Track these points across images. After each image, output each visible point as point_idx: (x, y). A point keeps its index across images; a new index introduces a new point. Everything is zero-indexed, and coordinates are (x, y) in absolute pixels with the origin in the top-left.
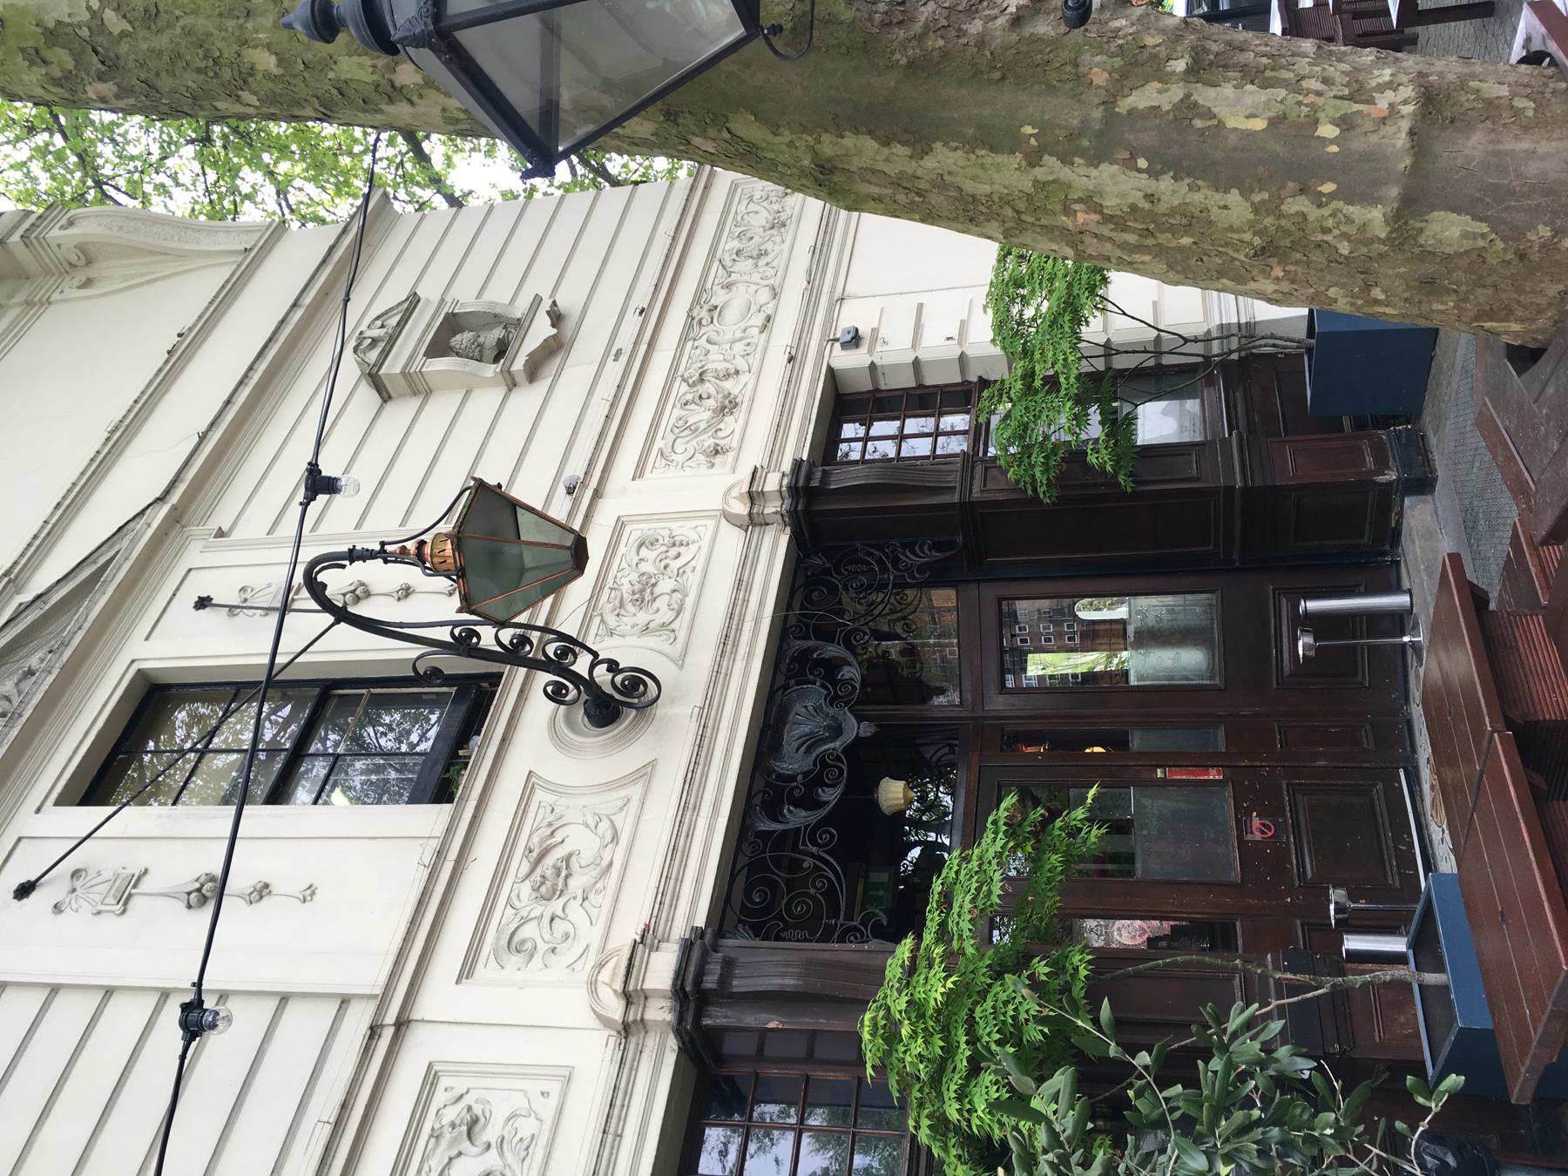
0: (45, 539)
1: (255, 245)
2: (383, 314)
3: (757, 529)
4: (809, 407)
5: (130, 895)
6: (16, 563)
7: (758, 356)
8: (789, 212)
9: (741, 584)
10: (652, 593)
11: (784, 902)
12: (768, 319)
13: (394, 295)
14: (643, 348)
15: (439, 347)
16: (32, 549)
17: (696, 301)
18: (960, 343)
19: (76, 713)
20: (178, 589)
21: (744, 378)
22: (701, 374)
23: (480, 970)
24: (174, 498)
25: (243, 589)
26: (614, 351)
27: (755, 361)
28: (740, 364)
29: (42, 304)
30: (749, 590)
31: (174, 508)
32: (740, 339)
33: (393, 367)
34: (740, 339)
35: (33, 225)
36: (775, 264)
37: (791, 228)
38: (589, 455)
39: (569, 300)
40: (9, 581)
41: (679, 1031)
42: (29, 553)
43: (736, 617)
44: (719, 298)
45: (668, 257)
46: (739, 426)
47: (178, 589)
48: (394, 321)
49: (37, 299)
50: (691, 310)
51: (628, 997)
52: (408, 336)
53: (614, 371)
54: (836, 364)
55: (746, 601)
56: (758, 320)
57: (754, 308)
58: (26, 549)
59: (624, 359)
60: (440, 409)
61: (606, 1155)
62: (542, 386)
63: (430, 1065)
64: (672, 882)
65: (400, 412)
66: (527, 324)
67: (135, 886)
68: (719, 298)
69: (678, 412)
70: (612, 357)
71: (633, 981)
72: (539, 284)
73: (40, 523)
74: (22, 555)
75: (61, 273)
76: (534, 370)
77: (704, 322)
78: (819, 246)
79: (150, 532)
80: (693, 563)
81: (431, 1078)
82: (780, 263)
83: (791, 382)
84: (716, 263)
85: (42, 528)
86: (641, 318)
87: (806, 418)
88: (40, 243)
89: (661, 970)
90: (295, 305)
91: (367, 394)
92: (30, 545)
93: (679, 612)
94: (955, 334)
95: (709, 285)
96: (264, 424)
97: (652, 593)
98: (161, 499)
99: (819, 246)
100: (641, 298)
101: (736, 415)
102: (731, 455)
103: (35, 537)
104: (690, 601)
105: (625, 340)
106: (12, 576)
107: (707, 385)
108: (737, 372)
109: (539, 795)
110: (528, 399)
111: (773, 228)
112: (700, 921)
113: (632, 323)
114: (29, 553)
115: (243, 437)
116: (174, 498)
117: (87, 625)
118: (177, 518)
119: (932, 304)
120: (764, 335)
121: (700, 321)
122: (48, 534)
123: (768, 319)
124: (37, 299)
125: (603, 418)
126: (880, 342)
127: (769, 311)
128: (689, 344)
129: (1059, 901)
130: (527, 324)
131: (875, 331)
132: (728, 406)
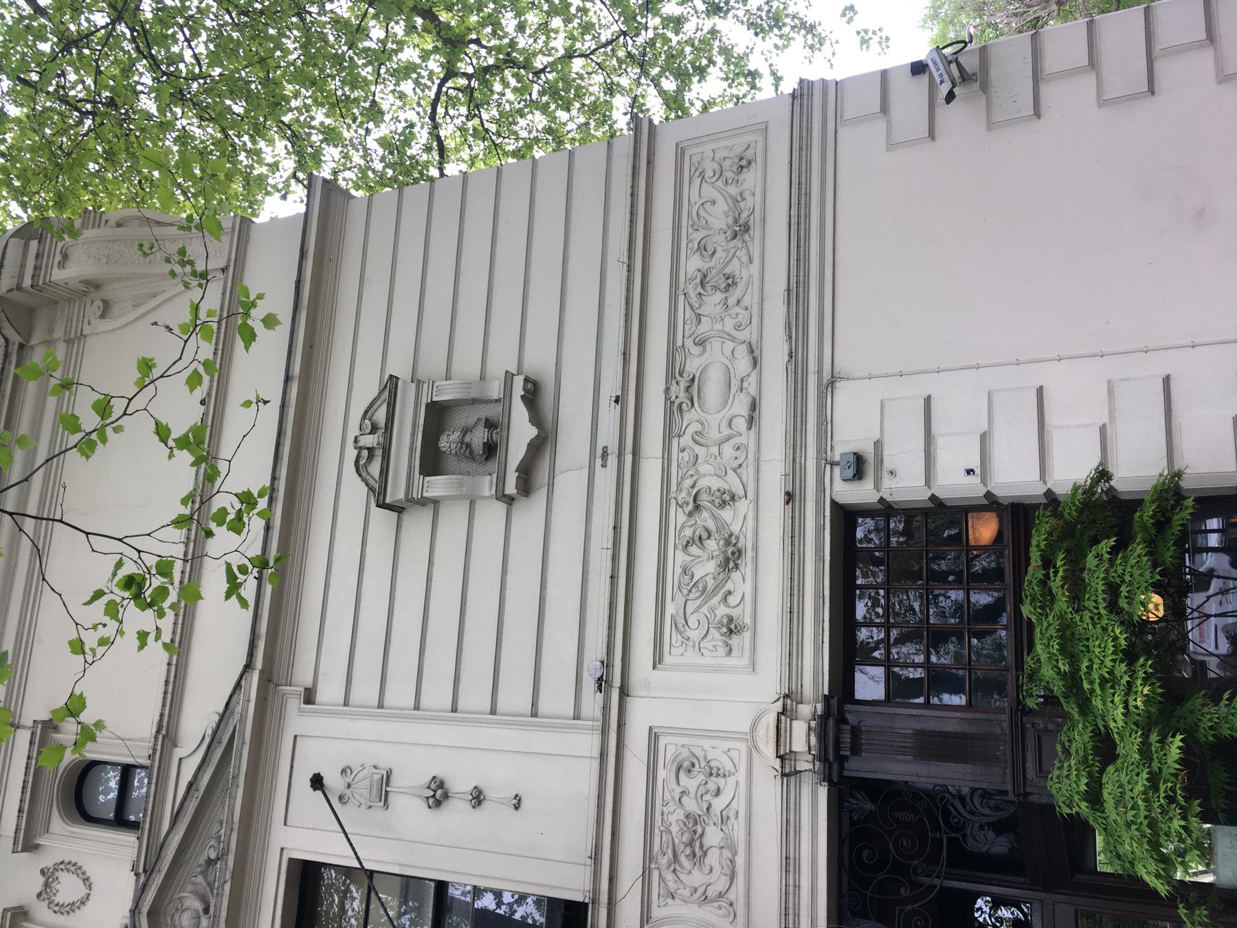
0: (174, 682)
1: (229, 260)
2: (366, 412)
3: (793, 778)
4: (819, 558)
5: (387, 792)
6: (162, 715)
7: (751, 469)
8: (750, 204)
9: (789, 864)
10: (701, 847)
11: (891, 847)
12: (754, 406)
13: (367, 389)
14: (629, 458)
15: (432, 463)
16: (169, 696)
17: (672, 373)
18: (984, 481)
19: (257, 910)
20: (293, 760)
21: (743, 506)
22: (695, 500)
23: (667, 659)
24: (259, 663)
25: (343, 771)
26: (599, 452)
27: (748, 473)
28: (735, 485)
29: (79, 339)
30: (797, 872)
31: (262, 672)
32: (729, 438)
33: (396, 493)
34: (729, 438)
35: (35, 268)
36: (746, 301)
37: (756, 232)
38: (605, 639)
39: (539, 360)
40: (164, 737)
41: (828, 778)
42: (168, 701)
43: (791, 912)
44: (692, 366)
45: (633, 213)
46: (748, 588)
47: (293, 760)
48: (381, 415)
49: (72, 336)
50: (667, 390)
51: (782, 758)
52: (403, 407)
53: (606, 479)
54: (842, 499)
55: (797, 887)
56: (740, 407)
57: (735, 384)
58: (165, 698)
59: (612, 461)
60: (453, 522)
61: (802, 245)
62: (540, 498)
63: (651, 728)
64: (791, 896)
65: (417, 525)
66: (506, 420)
67: (387, 785)
68: (692, 366)
69: (681, 557)
70: (599, 462)
71: (782, 748)
72: (503, 360)
73: (165, 667)
74: (164, 705)
75: (80, 298)
76: (526, 486)
77: (684, 406)
78: (793, 286)
79: (252, 706)
80: (734, 805)
81: (653, 737)
82: (751, 299)
83: (794, 535)
84: (681, 298)
85: (169, 671)
86: (619, 407)
87: (818, 595)
88: (49, 286)
89: (801, 737)
90: (288, 379)
91: (382, 520)
92: (165, 693)
93: (732, 877)
94: (975, 464)
95: (679, 343)
96: (305, 540)
97: (701, 847)
98: (248, 667)
99: (793, 286)
100: (611, 387)
101: (742, 567)
102: (747, 635)
103: (167, 682)
104: (740, 860)
105: (608, 436)
106: (164, 732)
107: (705, 514)
108: (733, 498)
109: (663, 741)
110: (529, 516)
111: (734, 237)
112: (826, 692)
113: (609, 416)
114: (168, 701)
115: (289, 593)
116: (259, 663)
117: (236, 826)
118: (268, 680)
119: (942, 389)
120: (752, 432)
121: (680, 405)
122: (175, 676)
123: (754, 406)
124: (72, 336)
125: (608, 580)
126: (886, 476)
127: (753, 390)
128: (675, 441)
129: (1147, 660)
130: (506, 420)
131: (878, 445)
132: (731, 559)
